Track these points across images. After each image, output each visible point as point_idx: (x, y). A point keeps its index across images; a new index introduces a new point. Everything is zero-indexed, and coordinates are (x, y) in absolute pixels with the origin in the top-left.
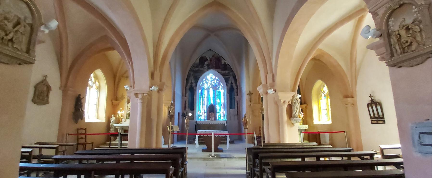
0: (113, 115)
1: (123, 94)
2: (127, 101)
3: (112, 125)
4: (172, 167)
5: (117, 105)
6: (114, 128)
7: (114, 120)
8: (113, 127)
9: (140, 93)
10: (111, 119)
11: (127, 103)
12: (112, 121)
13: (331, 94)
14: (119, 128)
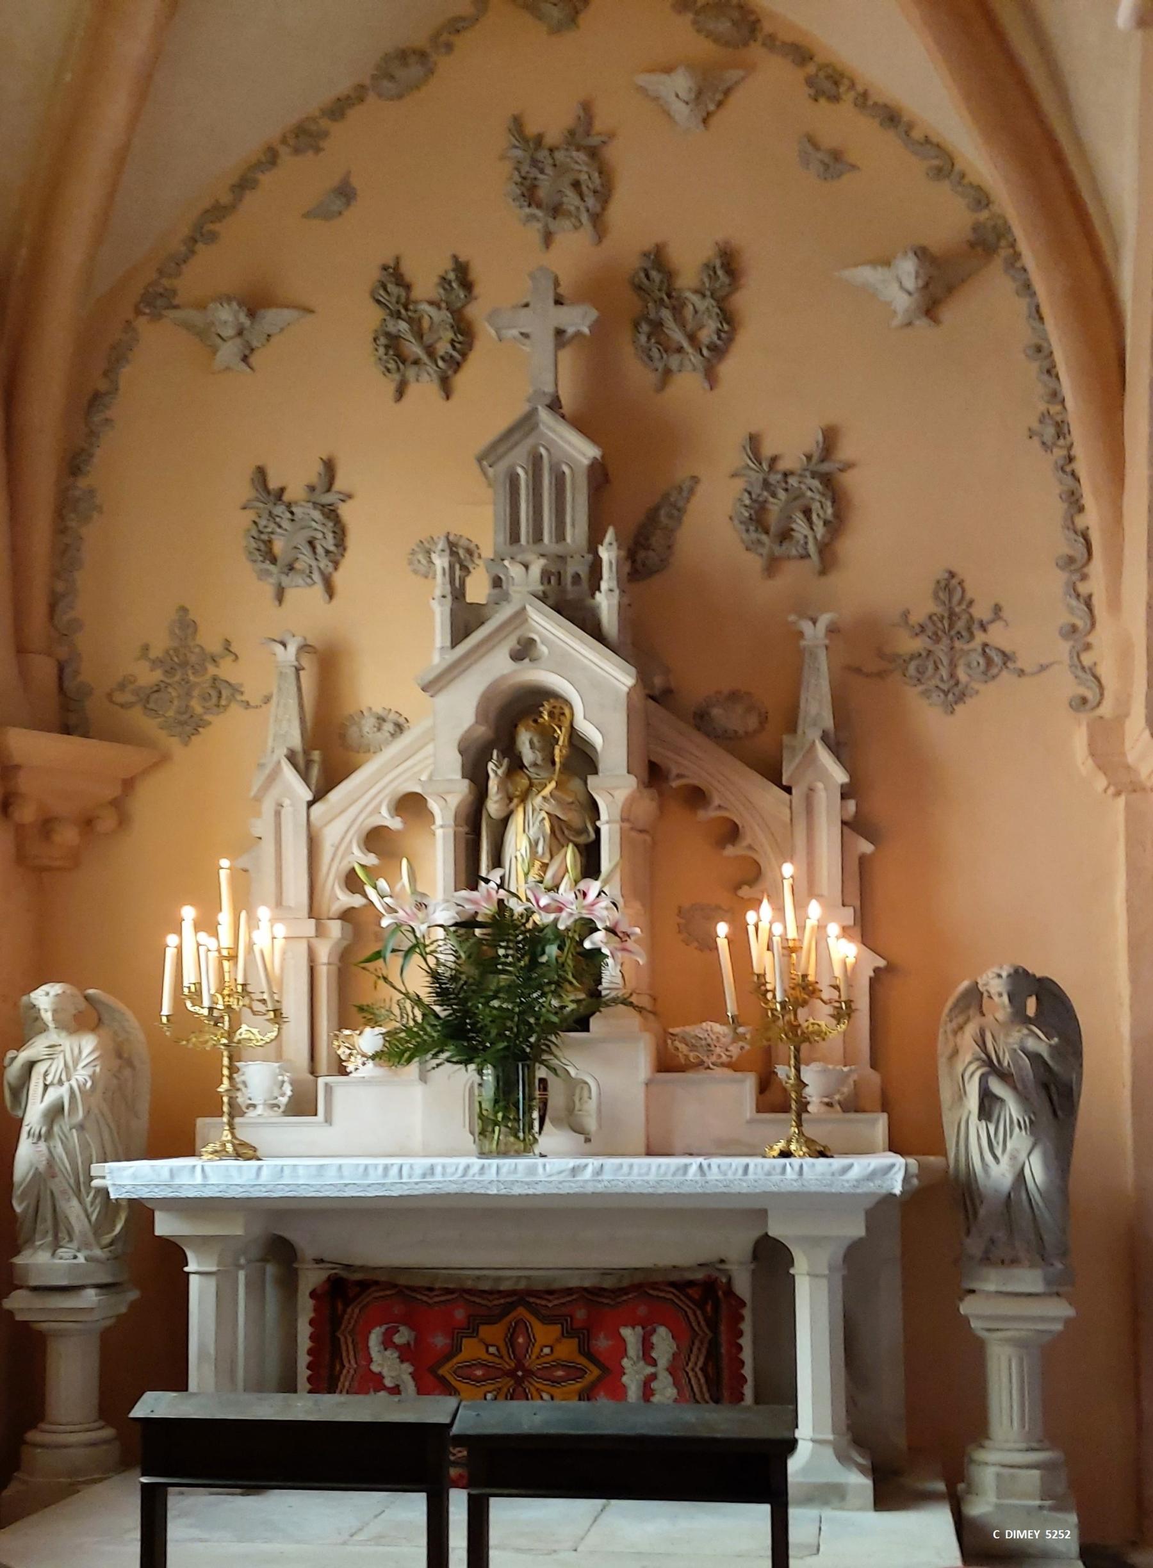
0: (45, 998)
1: (185, 625)
2: (295, 740)
3: (44, 1176)
4: (548, 701)
5: (88, 823)
6: (98, 1229)
7: (82, 1075)
8: (74, 1211)
9: (785, 927)
10: (13, 1072)
11: (289, 774)
12: (55, 1113)
13: (133, 1305)
14: (204, 1242)
